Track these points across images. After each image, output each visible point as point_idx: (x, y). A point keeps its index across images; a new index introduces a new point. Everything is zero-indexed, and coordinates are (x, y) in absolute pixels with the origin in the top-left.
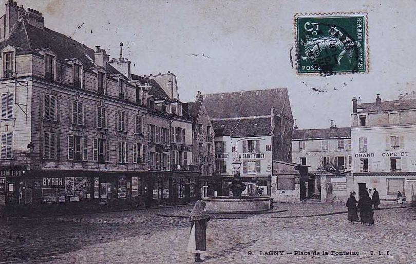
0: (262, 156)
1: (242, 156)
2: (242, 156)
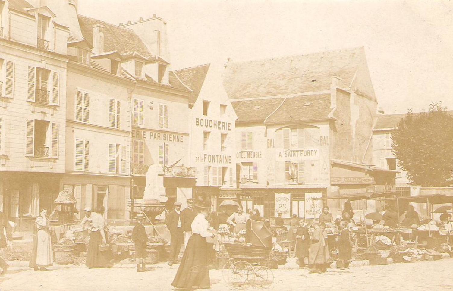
0: (314, 153)
2: (283, 155)
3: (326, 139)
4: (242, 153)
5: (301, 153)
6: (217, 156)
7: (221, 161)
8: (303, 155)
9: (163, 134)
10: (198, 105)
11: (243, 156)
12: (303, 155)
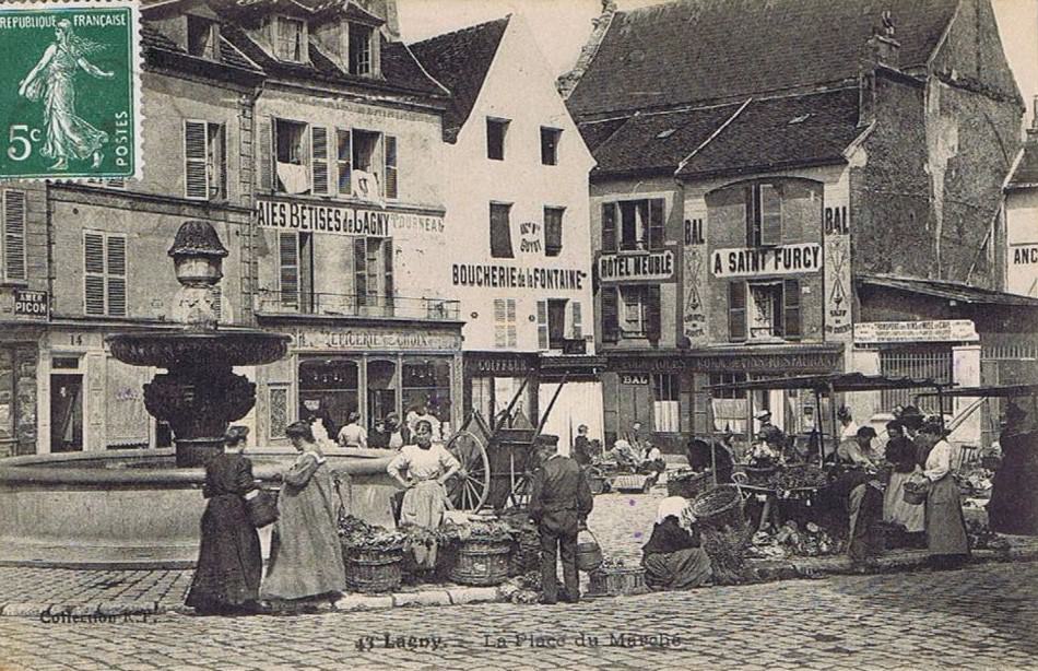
0: (810, 257)
1: (725, 264)
3: (841, 212)
4: (622, 260)
5: (778, 259)
6: (556, 271)
7: (562, 283)
8: (781, 264)
9: (370, 213)
10: (474, 131)
11: (623, 270)
12: (781, 264)
